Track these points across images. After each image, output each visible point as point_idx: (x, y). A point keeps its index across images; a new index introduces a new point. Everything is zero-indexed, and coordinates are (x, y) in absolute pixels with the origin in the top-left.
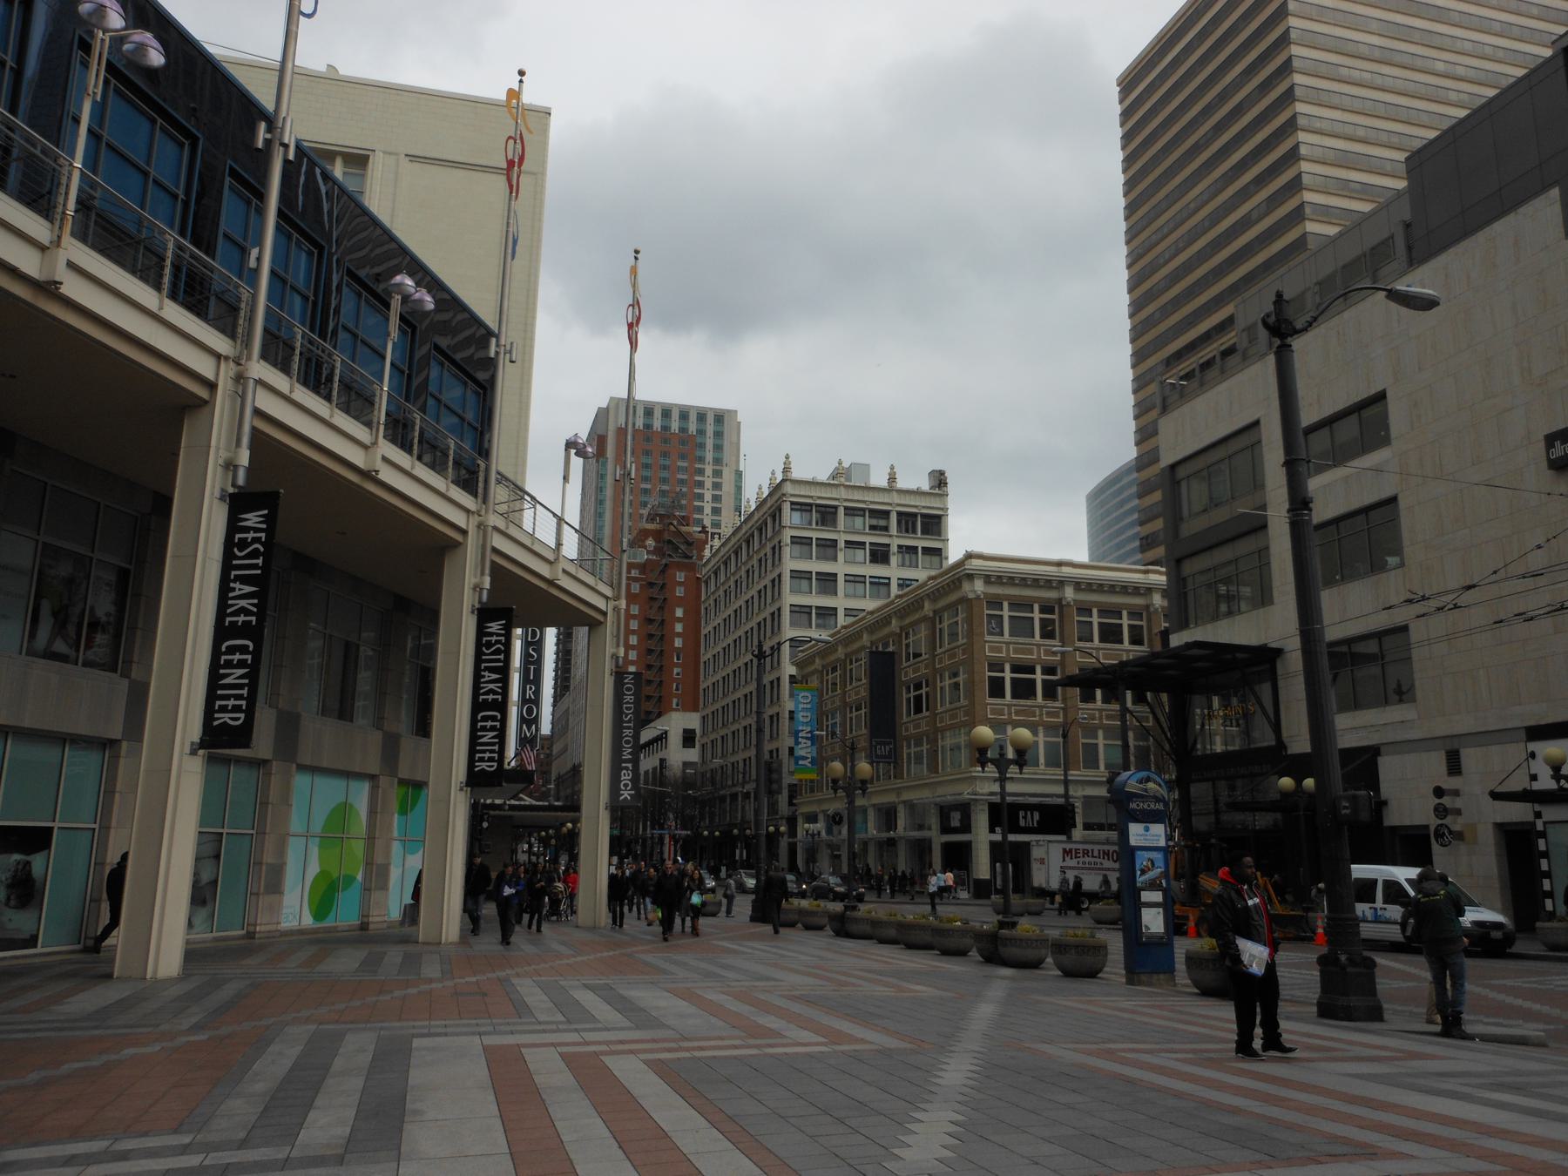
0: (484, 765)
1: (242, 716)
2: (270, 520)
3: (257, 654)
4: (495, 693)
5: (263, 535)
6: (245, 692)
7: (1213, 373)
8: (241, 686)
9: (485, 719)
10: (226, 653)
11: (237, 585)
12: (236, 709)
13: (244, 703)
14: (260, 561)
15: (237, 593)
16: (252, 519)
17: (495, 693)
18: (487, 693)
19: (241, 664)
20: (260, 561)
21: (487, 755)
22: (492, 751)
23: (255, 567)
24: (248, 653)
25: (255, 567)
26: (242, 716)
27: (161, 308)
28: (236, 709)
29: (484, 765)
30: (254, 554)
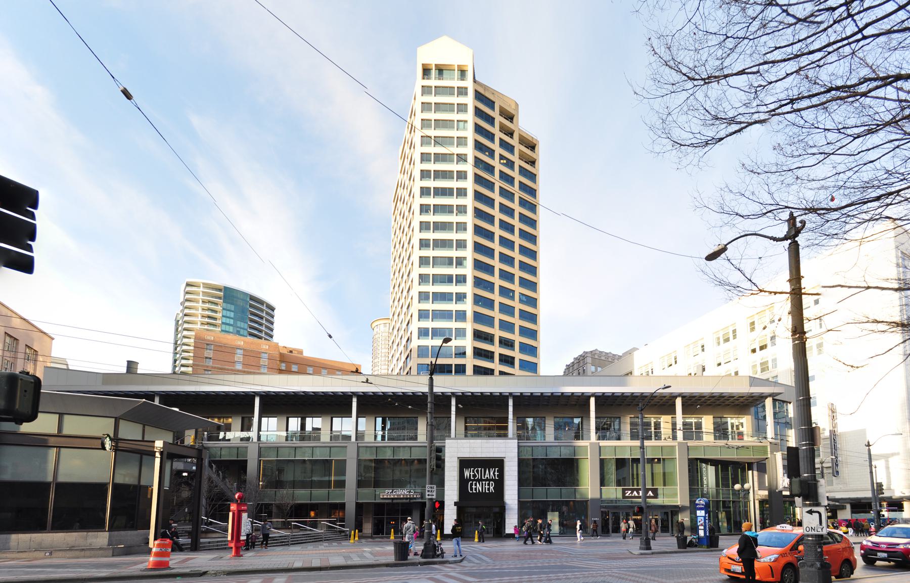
12: (489, 485)
28: (489, 485)
30: (477, 471)
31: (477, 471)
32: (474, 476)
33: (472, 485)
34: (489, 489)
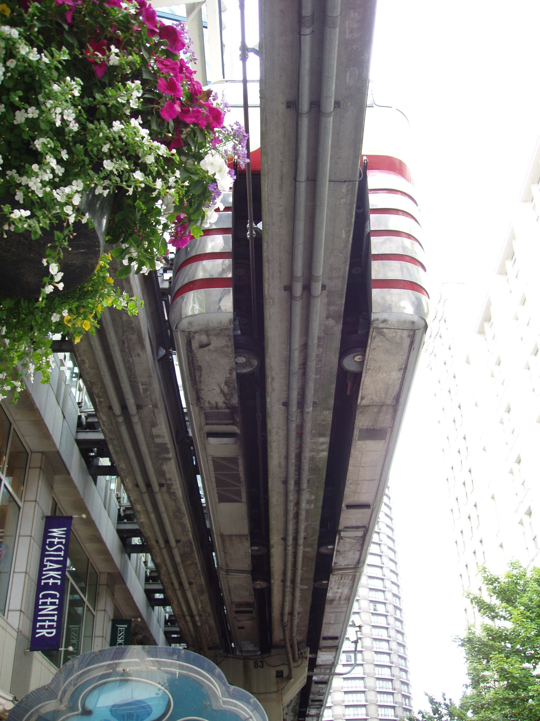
0: (44, 632)
1: (54, 631)
2: (68, 533)
3: (61, 599)
4: (54, 578)
5: (64, 541)
6: (55, 618)
7: (285, 388)
8: (53, 615)
9: (45, 596)
10: (43, 598)
11: (48, 564)
12: (50, 627)
13: (55, 624)
14: (62, 553)
15: (48, 568)
16: (57, 532)
17: (54, 578)
18: (49, 578)
19: (52, 604)
20: (62, 553)
21: (47, 623)
22: (50, 621)
23: (59, 556)
24: (57, 598)
25: (59, 556)
26: (54, 631)
27: (344, 652)
28: (50, 627)
29: (44, 632)
30: (59, 550)
31: (59, 550)
32: (52, 544)
33: (53, 596)
34: (42, 627)
